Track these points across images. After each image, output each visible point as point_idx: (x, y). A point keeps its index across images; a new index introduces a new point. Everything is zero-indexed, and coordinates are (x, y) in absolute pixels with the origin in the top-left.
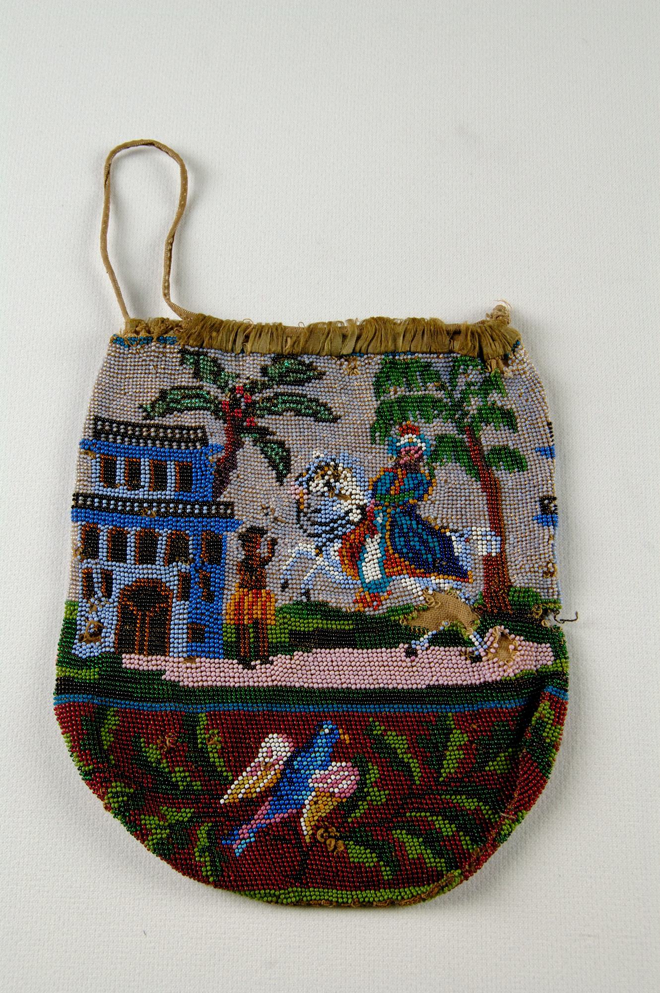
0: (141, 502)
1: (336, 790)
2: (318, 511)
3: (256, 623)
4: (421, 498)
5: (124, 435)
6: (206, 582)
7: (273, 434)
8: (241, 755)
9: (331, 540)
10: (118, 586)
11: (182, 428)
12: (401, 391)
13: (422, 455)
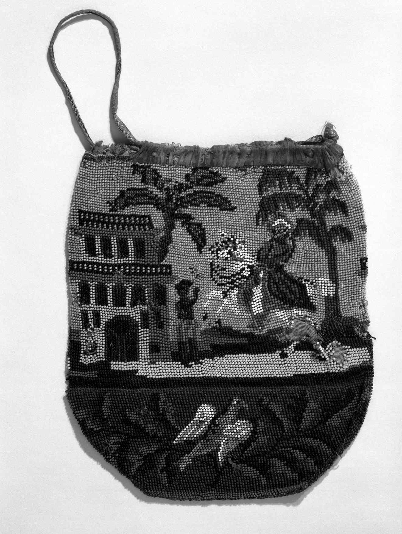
0: (114, 266)
1: (239, 436)
2: (224, 269)
3: (190, 339)
4: (286, 261)
5: (93, 221)
6: (158, 316)
7: (193, 219)
8: (186, 415)
9: (232, 288)
10: (104, 320)
11: (135, 216)
12: (277, 190)
13: (288, 233)
